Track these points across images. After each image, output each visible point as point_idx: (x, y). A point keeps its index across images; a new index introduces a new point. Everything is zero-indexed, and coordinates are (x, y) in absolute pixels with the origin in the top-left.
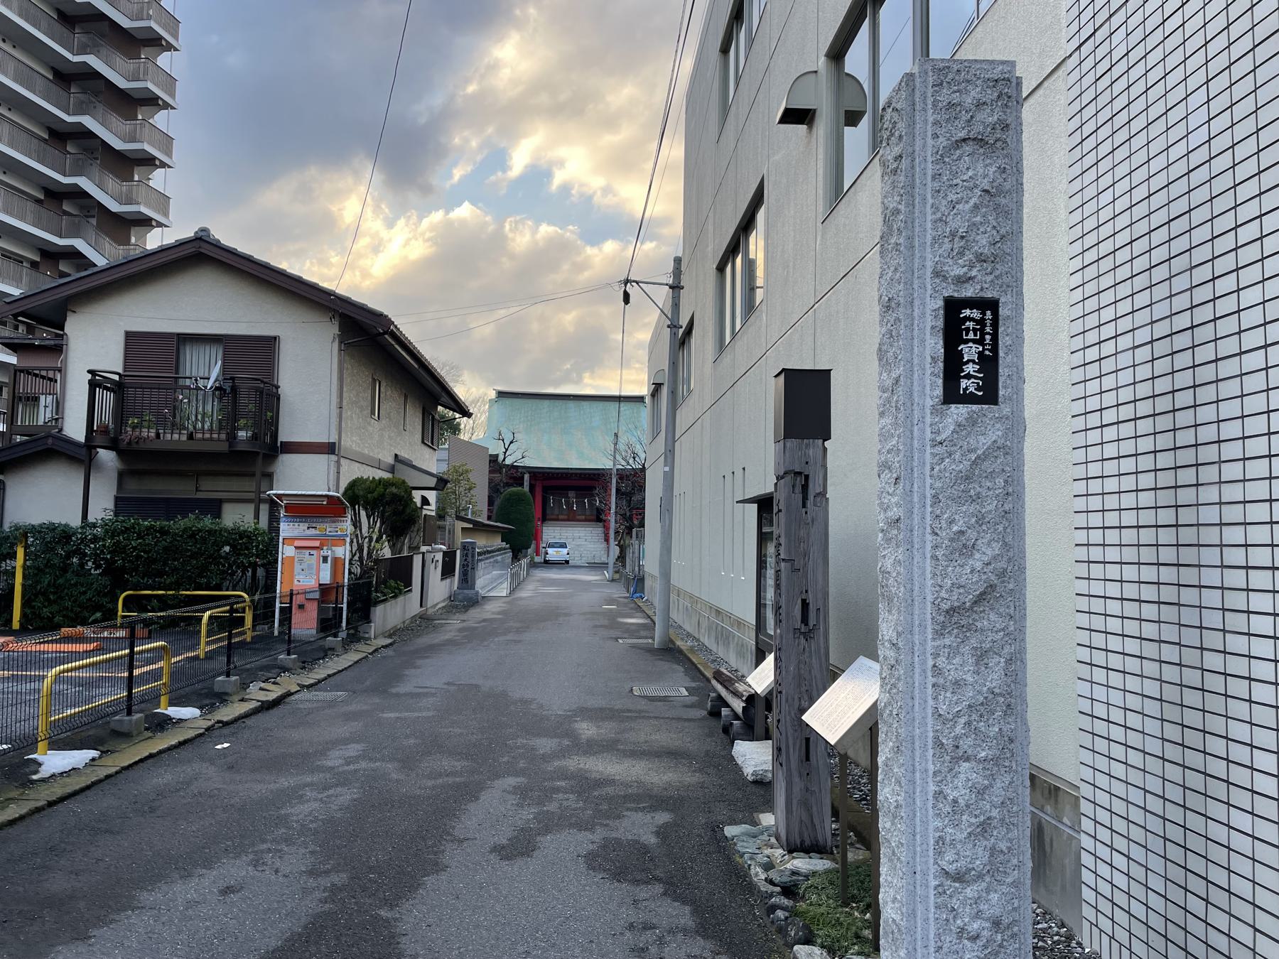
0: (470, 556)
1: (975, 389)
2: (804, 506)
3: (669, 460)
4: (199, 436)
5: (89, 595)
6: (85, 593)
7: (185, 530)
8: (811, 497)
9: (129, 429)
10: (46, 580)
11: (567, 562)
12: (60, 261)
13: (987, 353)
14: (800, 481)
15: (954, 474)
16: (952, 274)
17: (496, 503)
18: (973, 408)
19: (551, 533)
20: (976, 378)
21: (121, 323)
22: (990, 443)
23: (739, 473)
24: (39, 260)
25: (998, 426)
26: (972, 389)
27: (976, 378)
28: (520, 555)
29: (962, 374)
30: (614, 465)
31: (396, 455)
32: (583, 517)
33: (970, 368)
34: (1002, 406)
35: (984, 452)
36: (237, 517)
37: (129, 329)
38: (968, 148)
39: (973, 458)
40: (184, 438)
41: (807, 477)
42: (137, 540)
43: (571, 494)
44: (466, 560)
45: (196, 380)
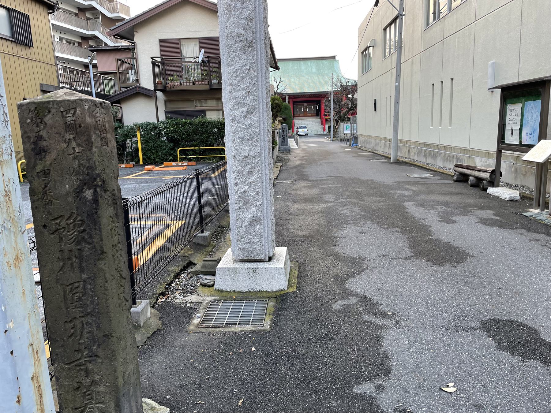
3: (398, 79)
4: (197, 83)
5: (167, 150)
6: (165, 149)
7: (199, 123)
9: (169, 82)
10: (150, 145)
11: (307, 134)
12: (86, 12)
19: (298, 122)
21: (157, 36)
23: (447, 83)
24: (78, 13)
30: (332, 89)
32: (311, 115)
36: (211, 116)
37: (160, 38)
40: (191, 84)
42: (181, 127)
44: (283, 133)
45: (195, 58)
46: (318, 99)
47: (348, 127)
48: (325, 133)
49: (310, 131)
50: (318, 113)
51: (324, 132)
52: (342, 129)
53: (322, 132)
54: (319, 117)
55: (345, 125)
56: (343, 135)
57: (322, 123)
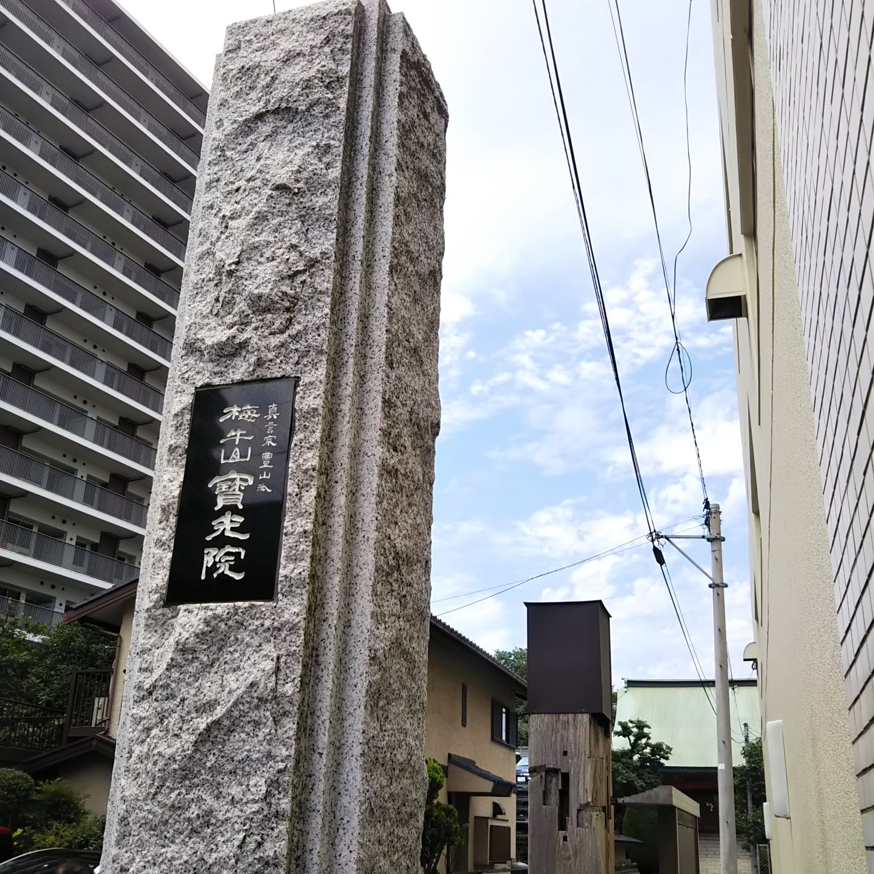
1: (231, 568)
2: (563, 826)
8: (573, 812)
13: (263, 488)
14: (556, 784)
15: (160, 765)
16: (209, 342)
18: (219, 611)
20: (235, 542)
22: (243, 689)
25: (268, 648)
26: (224, 569)
27: (235, 542)
29: (209, 538)
31: (449, 755)
33: (226, 524)
34: (282, 602)
35: (230, 711)
38: (265, 129)
39: (203, 726)
41: (566, 777)
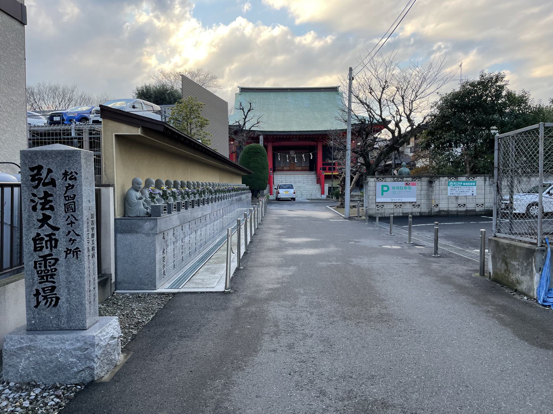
0: (59, 203)
11: (294, 199)
17: (240, 156)
28: (259, 195)
32: (300, 168)
43: (292, 153)
44: (45, 220)
46: (313, 143)
47: (385, 189)
48: (324, 197)
49: (298, 193)
50: (312, 167)
51: (323, 196)
52: (371, 193)
53: (319, 196)
54: (313, 172)
55: (379, 184)
56: (374, 206)
57: (319, 181)
